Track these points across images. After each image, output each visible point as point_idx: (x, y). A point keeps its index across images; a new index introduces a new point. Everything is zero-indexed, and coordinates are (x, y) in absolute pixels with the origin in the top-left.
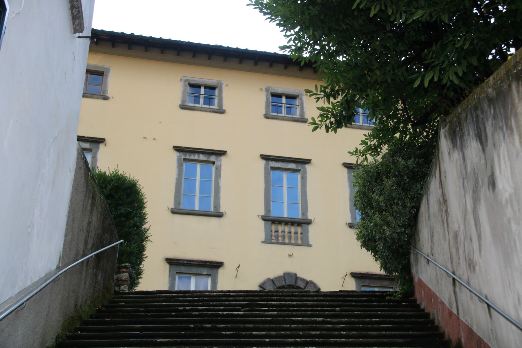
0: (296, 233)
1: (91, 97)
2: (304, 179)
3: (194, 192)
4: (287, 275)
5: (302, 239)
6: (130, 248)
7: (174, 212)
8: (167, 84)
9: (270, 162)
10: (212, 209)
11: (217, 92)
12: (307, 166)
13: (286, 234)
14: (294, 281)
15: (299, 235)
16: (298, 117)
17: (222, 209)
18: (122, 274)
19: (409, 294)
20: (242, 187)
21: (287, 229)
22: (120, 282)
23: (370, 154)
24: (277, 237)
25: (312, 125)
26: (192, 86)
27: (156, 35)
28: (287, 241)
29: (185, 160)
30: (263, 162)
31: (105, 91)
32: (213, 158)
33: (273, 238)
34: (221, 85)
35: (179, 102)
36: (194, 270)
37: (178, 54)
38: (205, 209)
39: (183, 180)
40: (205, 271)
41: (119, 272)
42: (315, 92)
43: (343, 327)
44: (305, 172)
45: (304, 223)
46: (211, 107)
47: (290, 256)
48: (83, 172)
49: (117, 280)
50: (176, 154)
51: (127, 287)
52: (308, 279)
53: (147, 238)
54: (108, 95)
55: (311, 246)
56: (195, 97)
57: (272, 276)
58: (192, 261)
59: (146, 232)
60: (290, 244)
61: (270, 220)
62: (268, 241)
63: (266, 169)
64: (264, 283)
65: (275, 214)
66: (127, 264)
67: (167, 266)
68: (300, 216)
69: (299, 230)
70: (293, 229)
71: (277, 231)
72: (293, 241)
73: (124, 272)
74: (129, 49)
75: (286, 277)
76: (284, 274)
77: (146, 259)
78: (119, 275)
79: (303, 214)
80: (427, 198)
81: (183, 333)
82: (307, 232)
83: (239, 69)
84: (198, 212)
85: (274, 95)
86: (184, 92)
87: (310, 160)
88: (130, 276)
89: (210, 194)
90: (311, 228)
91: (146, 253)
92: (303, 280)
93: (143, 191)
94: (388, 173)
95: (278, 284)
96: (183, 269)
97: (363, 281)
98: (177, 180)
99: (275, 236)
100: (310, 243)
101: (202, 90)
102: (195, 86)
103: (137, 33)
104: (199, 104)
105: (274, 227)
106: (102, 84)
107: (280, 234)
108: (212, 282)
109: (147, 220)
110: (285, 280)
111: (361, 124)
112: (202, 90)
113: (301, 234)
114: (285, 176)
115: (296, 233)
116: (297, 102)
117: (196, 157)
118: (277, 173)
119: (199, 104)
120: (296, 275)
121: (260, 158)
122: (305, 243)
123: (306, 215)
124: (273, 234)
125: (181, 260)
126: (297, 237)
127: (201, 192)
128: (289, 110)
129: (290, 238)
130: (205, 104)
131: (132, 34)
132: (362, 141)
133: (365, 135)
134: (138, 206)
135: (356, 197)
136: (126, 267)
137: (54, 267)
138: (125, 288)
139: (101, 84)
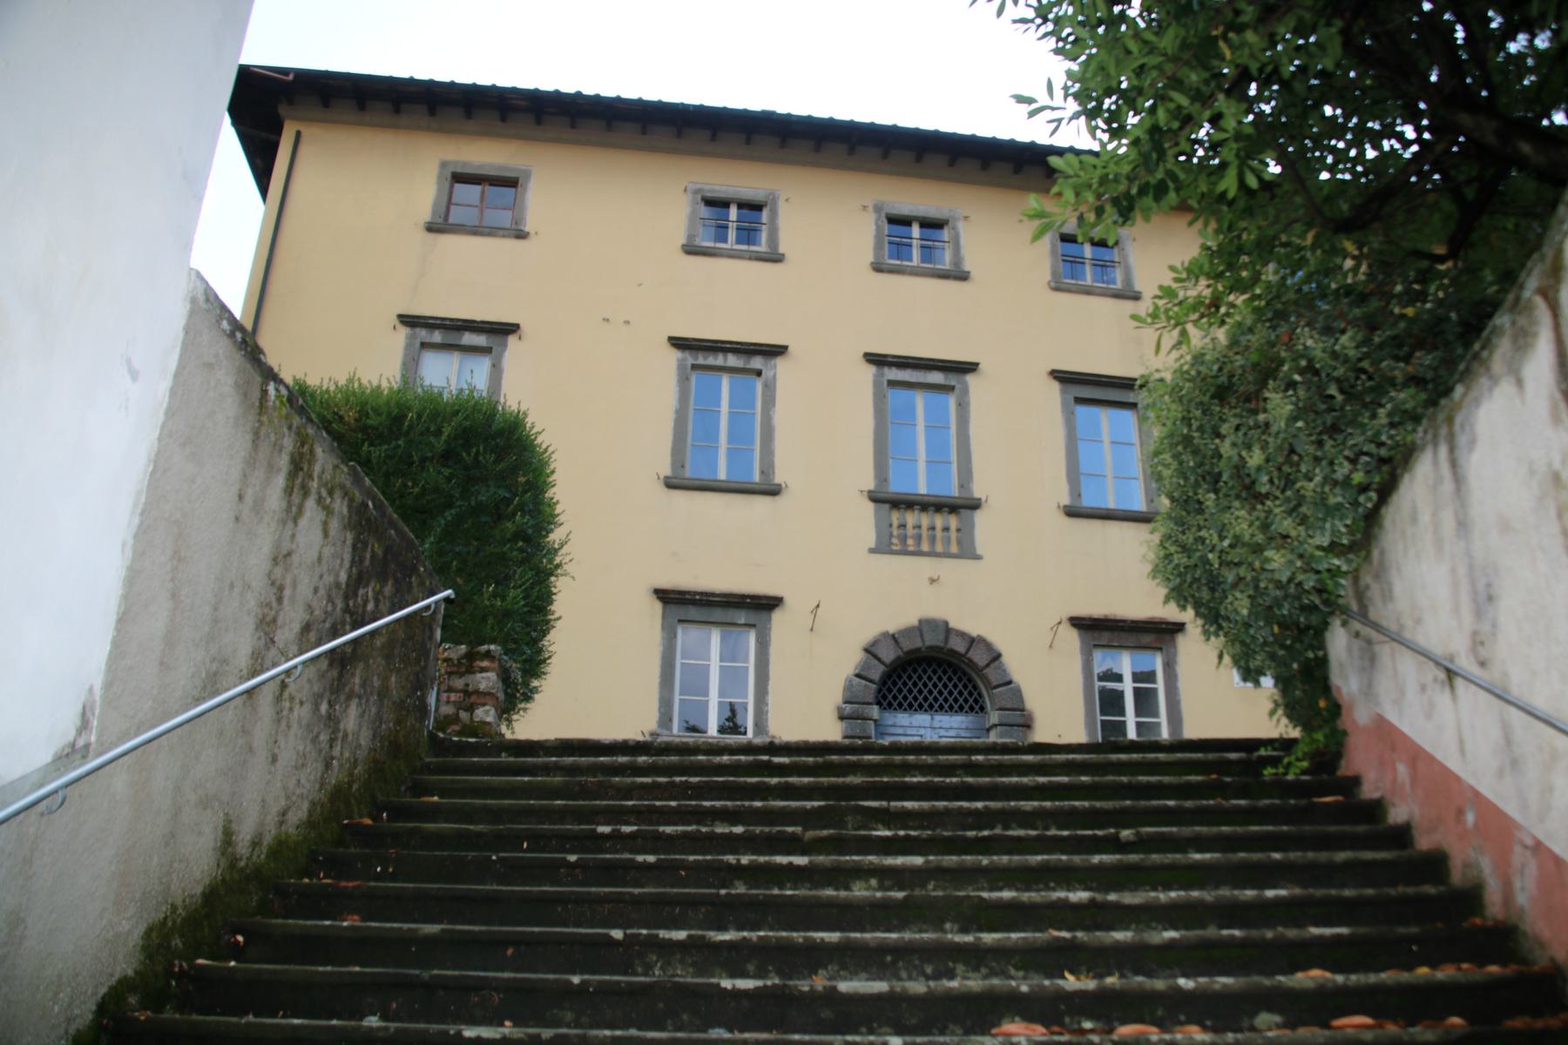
0: (946, 529)
1: (489, 235)
2: (963, 407)
3: (717, 440)
4: (926, 625)
5: (959, 542)
6: (504, 599)
7: (671, 484)
8: (652, 202)
9: (886, 370)
10: (757, 478)
11: (765, 215)
12: (970, 379)
13: (925, 533)
14: (942, 637)
15: (953, 535)
16: (947, 267)
17: (779, 478)
18: (479, 676)
19: (1327, 760)
20: (824, 426)
21: (925, 520)
22: (473, 699)
23: (1195, 322)
24: (903, 539)
25: (1031, 217)
26: (710, 202)
27: (630, 93)
28: (925, 547)
29: (695, 367)
30: (871, 370)
31: (518, 220)
32: (757, 363)
33: (895, 541)
34: (775, 200)
35: (682, 239)
36: (718, 614)
37: (679, 135)
38: (740, 478)
39: (691, 412)
40: (742, 617)
41: (470, 670)
42: (1048, 102)
43: (1173, 940)
44: (965, 391)
45: (962, 506)
46: (753, 248)
47: (932, 581)
48: (230, 381)
49: (466, 692)
50: (675, 355)
51: (493, 711)
52: (974, 633)
53: (558, 566)
54: (527, 229)
55: (979, 558)
56: (719, 227)
57: (892, 629)
58: (713, 595)
59: (556, 551)
60: (932, 554)
61: (889, 501)
62: (883, 547)
63: (877, 384)
64: (875, 643)
65: (897, 487)
66: (492, 647)
67: (658, 606)
68: (955, 492)
69: (953, 522)
70: (939, 520)
71: (903, 526)
72: (939, 548)
73: (483, 670)
74: (573, 126)
75: (925, 630)
76: (920, 621)
77: (558, 624)
78: (469, 679)
79: (961, 486)
80: (1454, 464)
81: (576, 980)
82: (972, 526)
83: (816, 164)
84: (724, 485)
85: (894, 220)
86: (692, 218)
87: (977, 364)
88: (505, 676)
89: (752, 442)
90: (979, 517)
91: (559, 606)
92: (962, 634)
93: (543, 440)
94: (1266, 372)
95: (907, 645)
96: (693, 612)
97: (1096, 635)
98: (677, 412)
99: (898, 537)
100: (979, 552)
101: (733, 212)
102: (717, 204)
103: (589, 91)
104: (725, 241)
105: (895, 517)
106: (516, 207)
107: (910, 531)
108: (757, 641)
109: (561, 519)
110: (922, 635)
111: (1089, 281)
112: (733, 212)
113: (958, 530)
114: (920, 400)
115: (946, 529)
116: (946, 234)
117: (719, 360)
118: (903, 394)
119: (725, 241)
120: (946, 623)
121: (863, 361)
122: (968, 552)
123: (969, 490)
124: (895, 532)
125: (688, 593)
126: (949, 539)
127: (731, 439)
128: (928, 252)
129: (933, 540)
130: (739, 241)
131: (579, 94)
132: (1161, 287)
133: (1172, 269)
134: (528, 482)
135: (1157, 453)
136: (488, 655)
137: (44, 756)
138: (487, 712)
139: (512, 207)
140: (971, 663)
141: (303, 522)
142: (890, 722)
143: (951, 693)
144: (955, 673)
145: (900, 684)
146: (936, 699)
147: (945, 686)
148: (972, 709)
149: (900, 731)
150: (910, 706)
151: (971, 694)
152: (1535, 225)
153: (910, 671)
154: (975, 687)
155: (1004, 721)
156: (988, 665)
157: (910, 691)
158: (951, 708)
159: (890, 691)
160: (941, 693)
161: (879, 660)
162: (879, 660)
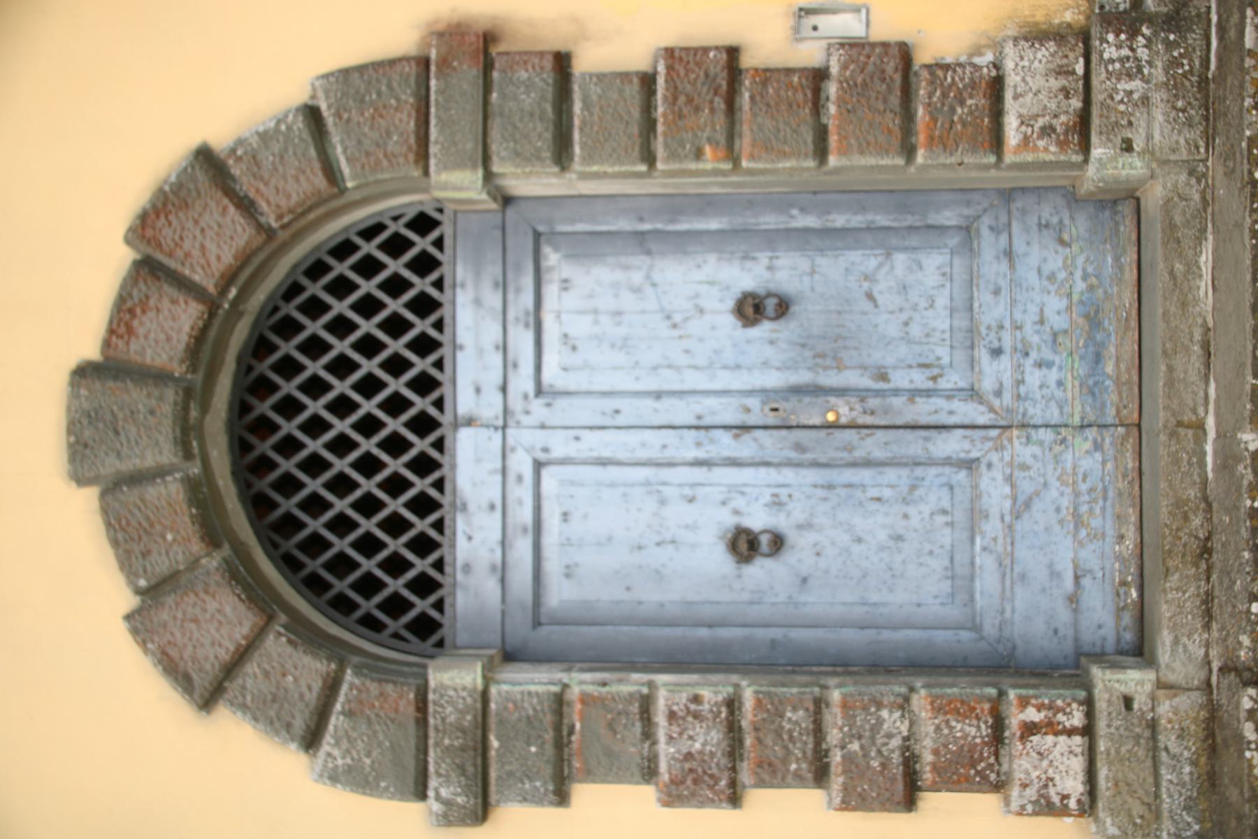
14: (138, 396)
52: (118, 258)
64: (174, 670)
75: (111, 466)
76: (80, 479)
95: (179, 541)
110: (137, 479)
120: (84, 373)
140: (242, 273)
141: (778, 374)
142: (491, 587)
143: (369, 346)
144: (288, 328)
145: (342, 544)
146: (396, 405)
147: (342, 367)
148: (425, 264)
149: (522, 548)
150: (424, 505)
151: (369, 267)
152: (142, 583)
153: (289, 505)
154: (343, 249)
155: (470, 145)
156: (246, 206)
157: (368, 505)
158: (424, 345)
159: (369, 585)
160: (369, 386)
161: (242, 655)
162: (242, 655)
